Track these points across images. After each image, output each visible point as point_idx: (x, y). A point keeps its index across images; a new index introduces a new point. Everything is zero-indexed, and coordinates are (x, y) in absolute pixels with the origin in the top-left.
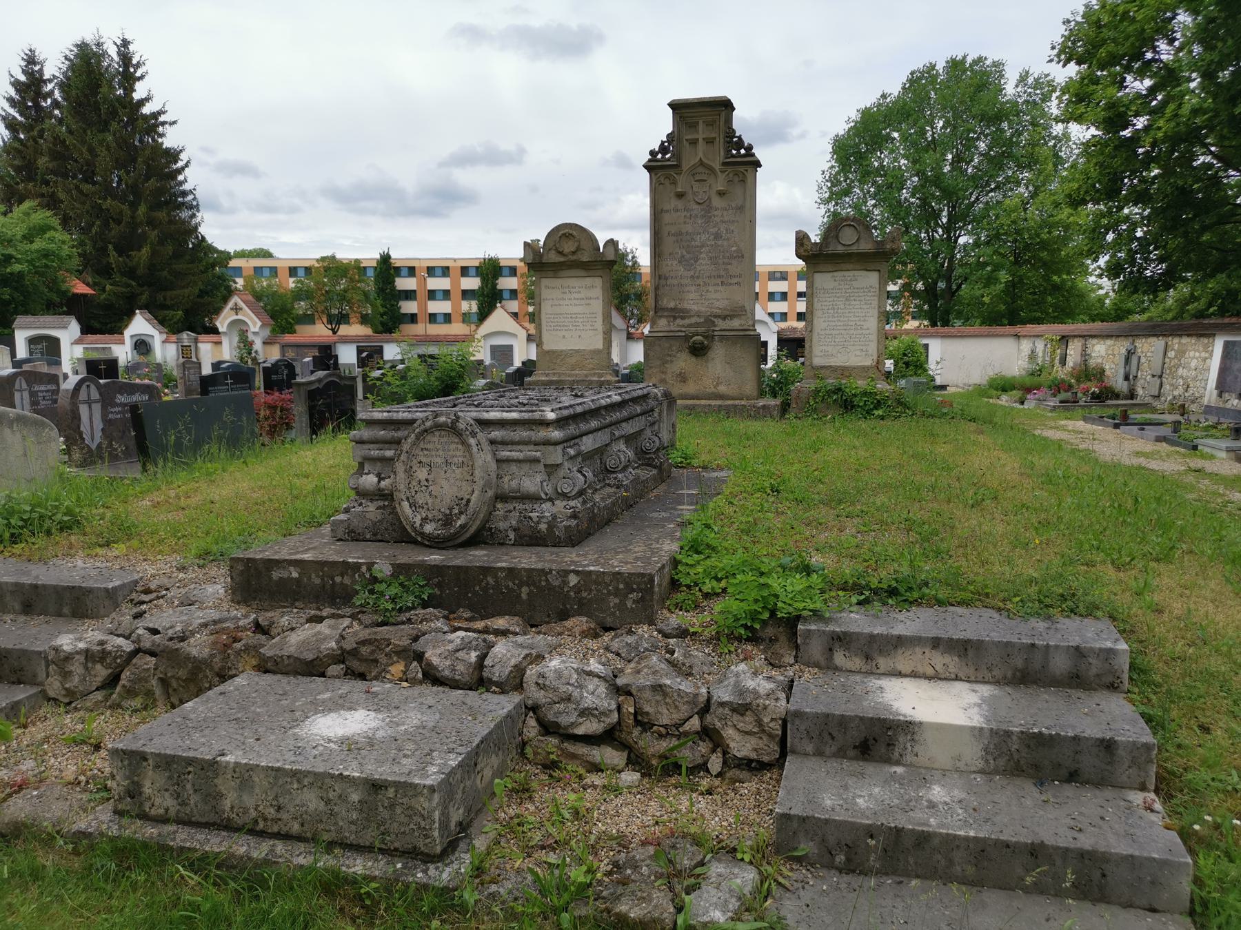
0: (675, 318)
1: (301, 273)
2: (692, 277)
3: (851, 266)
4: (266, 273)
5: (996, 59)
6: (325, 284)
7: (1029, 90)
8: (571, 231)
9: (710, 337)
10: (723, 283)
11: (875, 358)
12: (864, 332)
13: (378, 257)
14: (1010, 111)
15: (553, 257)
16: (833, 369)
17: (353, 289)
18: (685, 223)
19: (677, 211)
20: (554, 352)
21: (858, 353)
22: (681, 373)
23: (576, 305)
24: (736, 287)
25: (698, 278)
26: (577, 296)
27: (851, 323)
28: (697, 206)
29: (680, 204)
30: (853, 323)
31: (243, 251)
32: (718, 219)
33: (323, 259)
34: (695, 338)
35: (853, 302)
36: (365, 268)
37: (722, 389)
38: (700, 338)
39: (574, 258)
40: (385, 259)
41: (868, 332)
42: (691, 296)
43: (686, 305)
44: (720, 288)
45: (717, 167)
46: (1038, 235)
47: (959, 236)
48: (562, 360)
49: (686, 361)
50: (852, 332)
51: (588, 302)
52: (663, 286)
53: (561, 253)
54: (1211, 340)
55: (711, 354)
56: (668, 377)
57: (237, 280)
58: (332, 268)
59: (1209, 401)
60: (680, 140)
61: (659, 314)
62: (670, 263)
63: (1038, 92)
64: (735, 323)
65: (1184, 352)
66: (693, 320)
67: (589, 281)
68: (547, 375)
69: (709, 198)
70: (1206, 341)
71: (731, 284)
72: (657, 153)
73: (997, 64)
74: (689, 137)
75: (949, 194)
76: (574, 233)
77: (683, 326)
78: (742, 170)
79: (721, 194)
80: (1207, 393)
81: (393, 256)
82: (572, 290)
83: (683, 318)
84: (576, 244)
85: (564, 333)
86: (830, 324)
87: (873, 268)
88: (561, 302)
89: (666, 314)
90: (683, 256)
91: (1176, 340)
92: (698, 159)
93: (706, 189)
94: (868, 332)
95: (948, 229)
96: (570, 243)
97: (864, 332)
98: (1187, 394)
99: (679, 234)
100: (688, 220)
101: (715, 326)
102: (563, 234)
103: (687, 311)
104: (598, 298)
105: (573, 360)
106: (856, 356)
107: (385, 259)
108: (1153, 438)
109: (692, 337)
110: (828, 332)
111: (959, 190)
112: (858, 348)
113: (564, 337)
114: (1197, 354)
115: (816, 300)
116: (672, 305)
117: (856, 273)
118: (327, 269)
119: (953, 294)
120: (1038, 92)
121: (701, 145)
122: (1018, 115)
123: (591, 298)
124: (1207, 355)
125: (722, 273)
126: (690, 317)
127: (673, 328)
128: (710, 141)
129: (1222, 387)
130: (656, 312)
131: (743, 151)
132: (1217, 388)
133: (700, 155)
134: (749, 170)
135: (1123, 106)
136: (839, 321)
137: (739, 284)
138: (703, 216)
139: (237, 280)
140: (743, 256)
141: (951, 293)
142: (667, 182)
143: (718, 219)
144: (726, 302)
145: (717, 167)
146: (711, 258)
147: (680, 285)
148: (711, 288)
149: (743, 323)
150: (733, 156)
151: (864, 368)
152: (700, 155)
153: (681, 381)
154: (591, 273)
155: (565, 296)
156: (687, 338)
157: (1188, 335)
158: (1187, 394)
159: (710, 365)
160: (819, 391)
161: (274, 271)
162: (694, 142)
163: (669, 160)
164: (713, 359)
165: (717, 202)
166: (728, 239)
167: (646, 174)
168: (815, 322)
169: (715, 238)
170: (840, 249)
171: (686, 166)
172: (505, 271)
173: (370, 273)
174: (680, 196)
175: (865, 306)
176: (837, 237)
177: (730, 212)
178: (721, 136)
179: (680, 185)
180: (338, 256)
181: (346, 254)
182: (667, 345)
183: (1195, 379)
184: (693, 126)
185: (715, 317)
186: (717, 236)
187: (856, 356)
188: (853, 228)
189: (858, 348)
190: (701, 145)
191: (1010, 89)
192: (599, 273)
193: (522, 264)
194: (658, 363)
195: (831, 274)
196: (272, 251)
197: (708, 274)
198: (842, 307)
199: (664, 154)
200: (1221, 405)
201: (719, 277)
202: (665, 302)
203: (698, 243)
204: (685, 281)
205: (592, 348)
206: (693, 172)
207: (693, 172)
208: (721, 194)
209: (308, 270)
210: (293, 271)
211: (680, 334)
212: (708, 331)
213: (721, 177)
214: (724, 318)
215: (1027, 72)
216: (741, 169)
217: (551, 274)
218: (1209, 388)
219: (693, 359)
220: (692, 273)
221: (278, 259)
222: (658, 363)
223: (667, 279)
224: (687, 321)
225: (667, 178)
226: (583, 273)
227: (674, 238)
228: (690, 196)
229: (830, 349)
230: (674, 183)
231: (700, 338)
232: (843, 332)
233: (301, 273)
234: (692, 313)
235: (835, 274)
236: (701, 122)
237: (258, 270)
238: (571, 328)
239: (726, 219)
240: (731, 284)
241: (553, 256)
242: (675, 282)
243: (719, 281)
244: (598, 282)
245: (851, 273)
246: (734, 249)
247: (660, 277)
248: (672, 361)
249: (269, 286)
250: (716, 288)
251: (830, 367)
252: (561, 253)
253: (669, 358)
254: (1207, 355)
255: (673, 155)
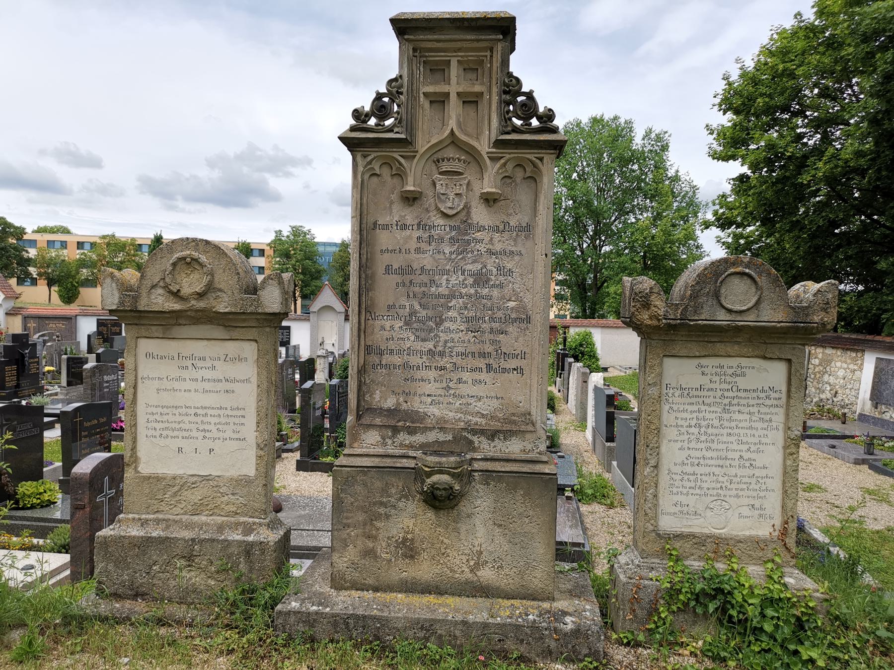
0: (396, 430)
1: (87, 246)
2: (431, 353)
3: (729, 349)
4: (58, 245)
5: (628, 118)
6: (105, 257)
7: (652, 143)
8: (196, 255)
9: (465, 476)
10: (489, 367)
11: (778, 522)
12: (757, 472)
13: (153, 237)
14: (638, 157)
15: (159, 301)
16: (699, 540)
17: (129, 261)
18: (418, 250)
19: (404, 227)
20: (158, 479)
21: (746, 511)
22: (405, 540)
23: (205, 391)
24: (514, 376)
25: (442, 354)
26: (208, 374)
27: (730, 455)
28: (441, 222)
29: (410, 216)
30: (736, 455)
31: (45, 227)
32: (482, 247)
33: (104, 237)
34: (435, 478)
35: (736, 416)
36: (140, 245)
37: (487, 575)
38: (445, 478)
39: (201, 304)
40: (158, 240)
41: (764, 473)
42: (430, 388)
43: (417, 405)
44: (483, 376)
45: (484, 147)
46: (663, 249)
47: (603, 246)
48: (175, 494)
49: (415, 516)
50: (733, 471)
51: (229, 386)
52: (374, 367)
53: (176, 295)
54: (859, 355)
55: (465, 507)
56: (382, 549)
57: (30, 250)
58: (114, 245)
59: (863, 409)
60: (413, 95)
61: (366, 420)
62: (388, 324)
63: (659, 144)
64: (514, 447)
65: (830, 362)
66: (432, 436)
67: (232, 348)
68: (144, 523)
69: (467, 208)
70: (854, 355)
71: (504, 370)
72: (368, 116)
73: (629, 123)
74: (430, 89)
75: (597, 215)
76: (203, 258)
77: (411, 446)
78: (531, 157)
79: (489, 200)
80: (859, 401)
81: (164, 237)
82: (200, 364)
83: (411, 431)
84: (205, 280)
85: (180, 443)
86: (694, 454)
87: (778, 354)
88: (176, 385)
89: (378, 421)
90: (413, 313)
91: (819, 350)
92: (448, 132)
93: (463, 190)
94: (764, 473)
95: (593, 239)
96: (195, 276)
97: (757, 472)
98: (835, 399)
99: (406, 270)
100: (423, 246)
101: (474, 450)
102: (181, 259)
103: (424, 417)
104: (248, 381)
105: (195, 496)
106: (741, 516)
107: (158, 240)
108: (852, 460)
109: (429, 475)
110: (689, 469)
111: (605, 212)
112: (746, 501)
113: (180, 450)
114: (845, 366)
115: (666, 407)
116: (390, 403)
117: (744, 362)
118: (108, 244)
119: (599, 289)
120: (659, 144)
121: (454, 107)
122: (645, 160)
123: (235, 381)
124: (856, 367)
125: (489, 348)
126: (426, 429)
127: (391, 451)
128: (470, 100)
129: (877, 397)
130: (359, 417)
131: (535, 122)
132: (872, 399)
133: (452, 124)
134: (547, 158)
135: (781, 148)
136: (708, 449)
137: (519, 370)
138: (453, 240)
139: (30, 250)
140: (528, 320)
141: (598, 286)
142: (386, 172)
143: (482, 247)
144: (495, 404)
145: (484, 147)
146: (468, 320)
147: (406, 366)
148: (466, 376)
149: (529, 447)
150: (516, 130)
151: (758, 543)
152: (452, 124)
153: (405, 556)
154: (236, 334)
155: (185, 374)
156: (419, 474)
157: (833, 348)
158: (835, 399)
159: (463, 528)
160: (679, 591)
161: (64, 245)
162: (439, 101)
163: (390, 130)
164: (469, 516)
165: (480, 215)
166: (501, 286)
167: (346, 156)
168: (664, 449)
169: (476, 283)
170: (722, 318)
171: (422, 144)
172: (256, 253)
173: (145, 249)
174: (411, 199)
175: (760, 425)
176: (717, 295)
177: (506, 235)
178: (495, 90)
179: (410, 179)
180: (117, 235)
181: (123, 233)
182: (378, 484)
183: (844, 387)
184: (439, 70)
185: (474, 432)
186: (481, 279)
187: (741, 516)
188: (749, 281)
189: (746, 501)
190: (454, 107)
191: (638, 141)
192: (253, 334)
193: (268, 248)
194: (361, 517)
195: (696, 362)
196: (70, 228)
197: (460, 349)
198: (716, 423)
199: (382, 117)
200: (877, 415)
201: (483, 355)
202: (377, 396)
203: (443, 290)
204: (415, 360)
205: (233, 473)
206: (436, 157)
207: (436, 157)
208: (489, 200)
209: (93, 245)
210: (80, 245)
211: (405, 463)
212: (460, 464)
213: (492, 169)
214: (492, 435)
215: (651, 130)
216: (531, 155)
217: (156, 331)
218: (861, 396)
219: (430, 514)
220: (430, 345)
221: (76, 235)
222: (361, 517)
223: (381, 354)
224: (419, 438)
225: (388, 163)
226: (219, 332)
227: (398, 278)
228: (429, 201)
229: (691, 500)
230: (400, 175)
231: (445, 478)
232: (717, 471)
233: (87, 246)
234: (429, 422)
235: (704, 361)
236: (454, 63)
237: (50, 243)
238: (194, 434)
239: (498, 247)
240: (504, 370)
241: (160, 300)
242: (397, 360)
243: (481, 363)
244: (249, 350)
245: (734, 362)
246: (511, 304)
247: (368, 350)
248: (388, 516)
249: (57, 256)
250: (477, 376)
251: (693, 536)
252: (176, 295)
253: (382, 510)
254: (856, 367)
255: (399, 121)
